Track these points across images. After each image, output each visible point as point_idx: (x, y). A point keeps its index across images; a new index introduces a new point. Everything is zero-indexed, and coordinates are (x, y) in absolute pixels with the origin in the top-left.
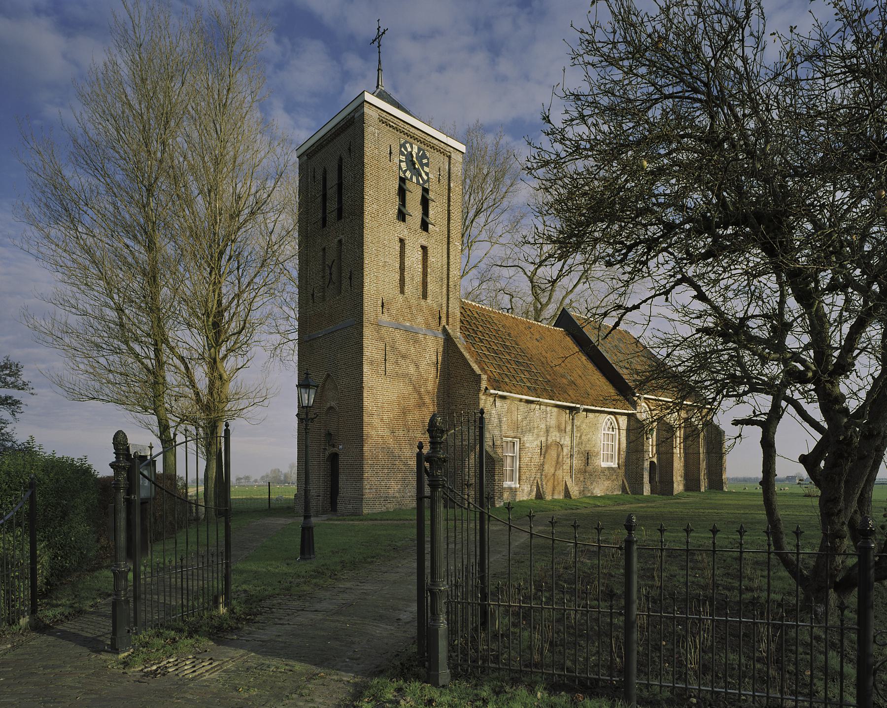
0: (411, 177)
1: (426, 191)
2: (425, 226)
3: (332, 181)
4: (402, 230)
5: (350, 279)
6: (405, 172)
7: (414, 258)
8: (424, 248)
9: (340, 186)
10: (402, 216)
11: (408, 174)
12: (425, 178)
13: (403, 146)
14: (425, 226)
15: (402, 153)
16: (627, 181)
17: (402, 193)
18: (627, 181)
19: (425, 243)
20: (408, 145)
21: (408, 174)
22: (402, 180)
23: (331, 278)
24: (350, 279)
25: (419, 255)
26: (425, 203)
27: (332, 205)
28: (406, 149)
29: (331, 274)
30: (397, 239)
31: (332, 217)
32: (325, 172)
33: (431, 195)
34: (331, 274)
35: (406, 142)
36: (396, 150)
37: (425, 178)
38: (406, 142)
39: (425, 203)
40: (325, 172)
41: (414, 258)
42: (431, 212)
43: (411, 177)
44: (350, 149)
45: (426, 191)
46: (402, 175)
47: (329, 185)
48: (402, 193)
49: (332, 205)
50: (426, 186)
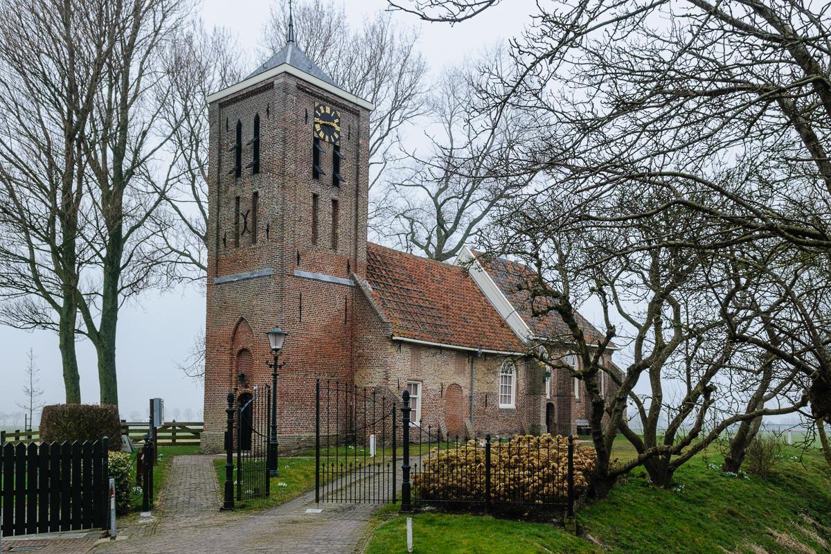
0: (324, 137)
1: (337, 148)
2: (336, 182)
3: (248, 136)
4: (317, 189)
5: (268, 231)
6: (318, 133)
7: (325, 208)
8: (335, 202)
9: (256, 144)
10: (316, 174)
11: (322, 134)
12: (337, 136)
13: (318, 108)
14: (336, 182)
15: (316, 115)
16: (702, 393)
17: (316, 153)
18: (702, 393)
19: (336, 197)
20: (321, 108)
21: (322, 134)
22: (317, 140)
23: (246, 227)
24: (268, 231)
25: (330, 208)
26: (336, 160)
27: (247, 159)
28: (320, 111)
29: (246, 223)
30: (311, 195)
31: (246, 171)
32: (239, 126)
33: (342, 152)
34: (246, 223)
35: (320, 105)
36: (311, 113)
37: (337, 136)
38: (320, 105)
39: (336, 160)
40: (239, 126)
41: (325, 208)
42: (341, 169)
43: (324, 137)
44: (268, 110)
45: (337, 148)
46: (316, 135)
47: (397, 490)
48: (316, 153)
49: (247, 159)
50: (337, 144)
